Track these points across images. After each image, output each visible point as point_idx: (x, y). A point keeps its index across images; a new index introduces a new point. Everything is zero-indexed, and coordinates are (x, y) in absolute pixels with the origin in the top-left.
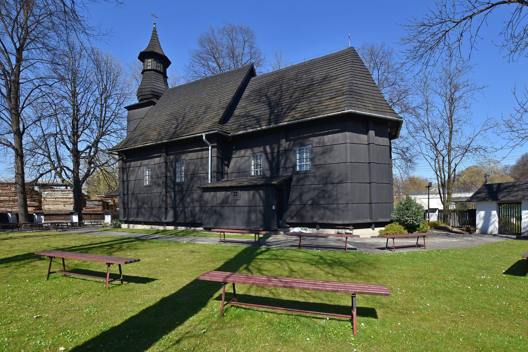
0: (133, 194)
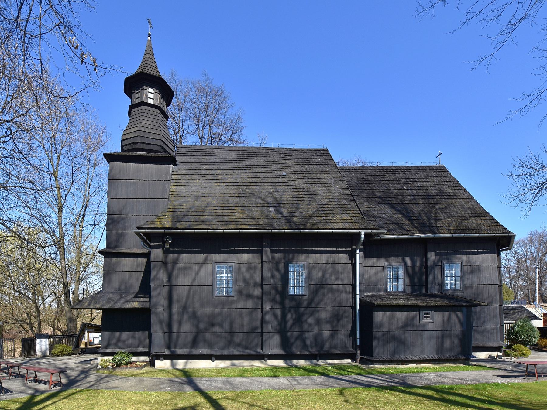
0: (185, 308)
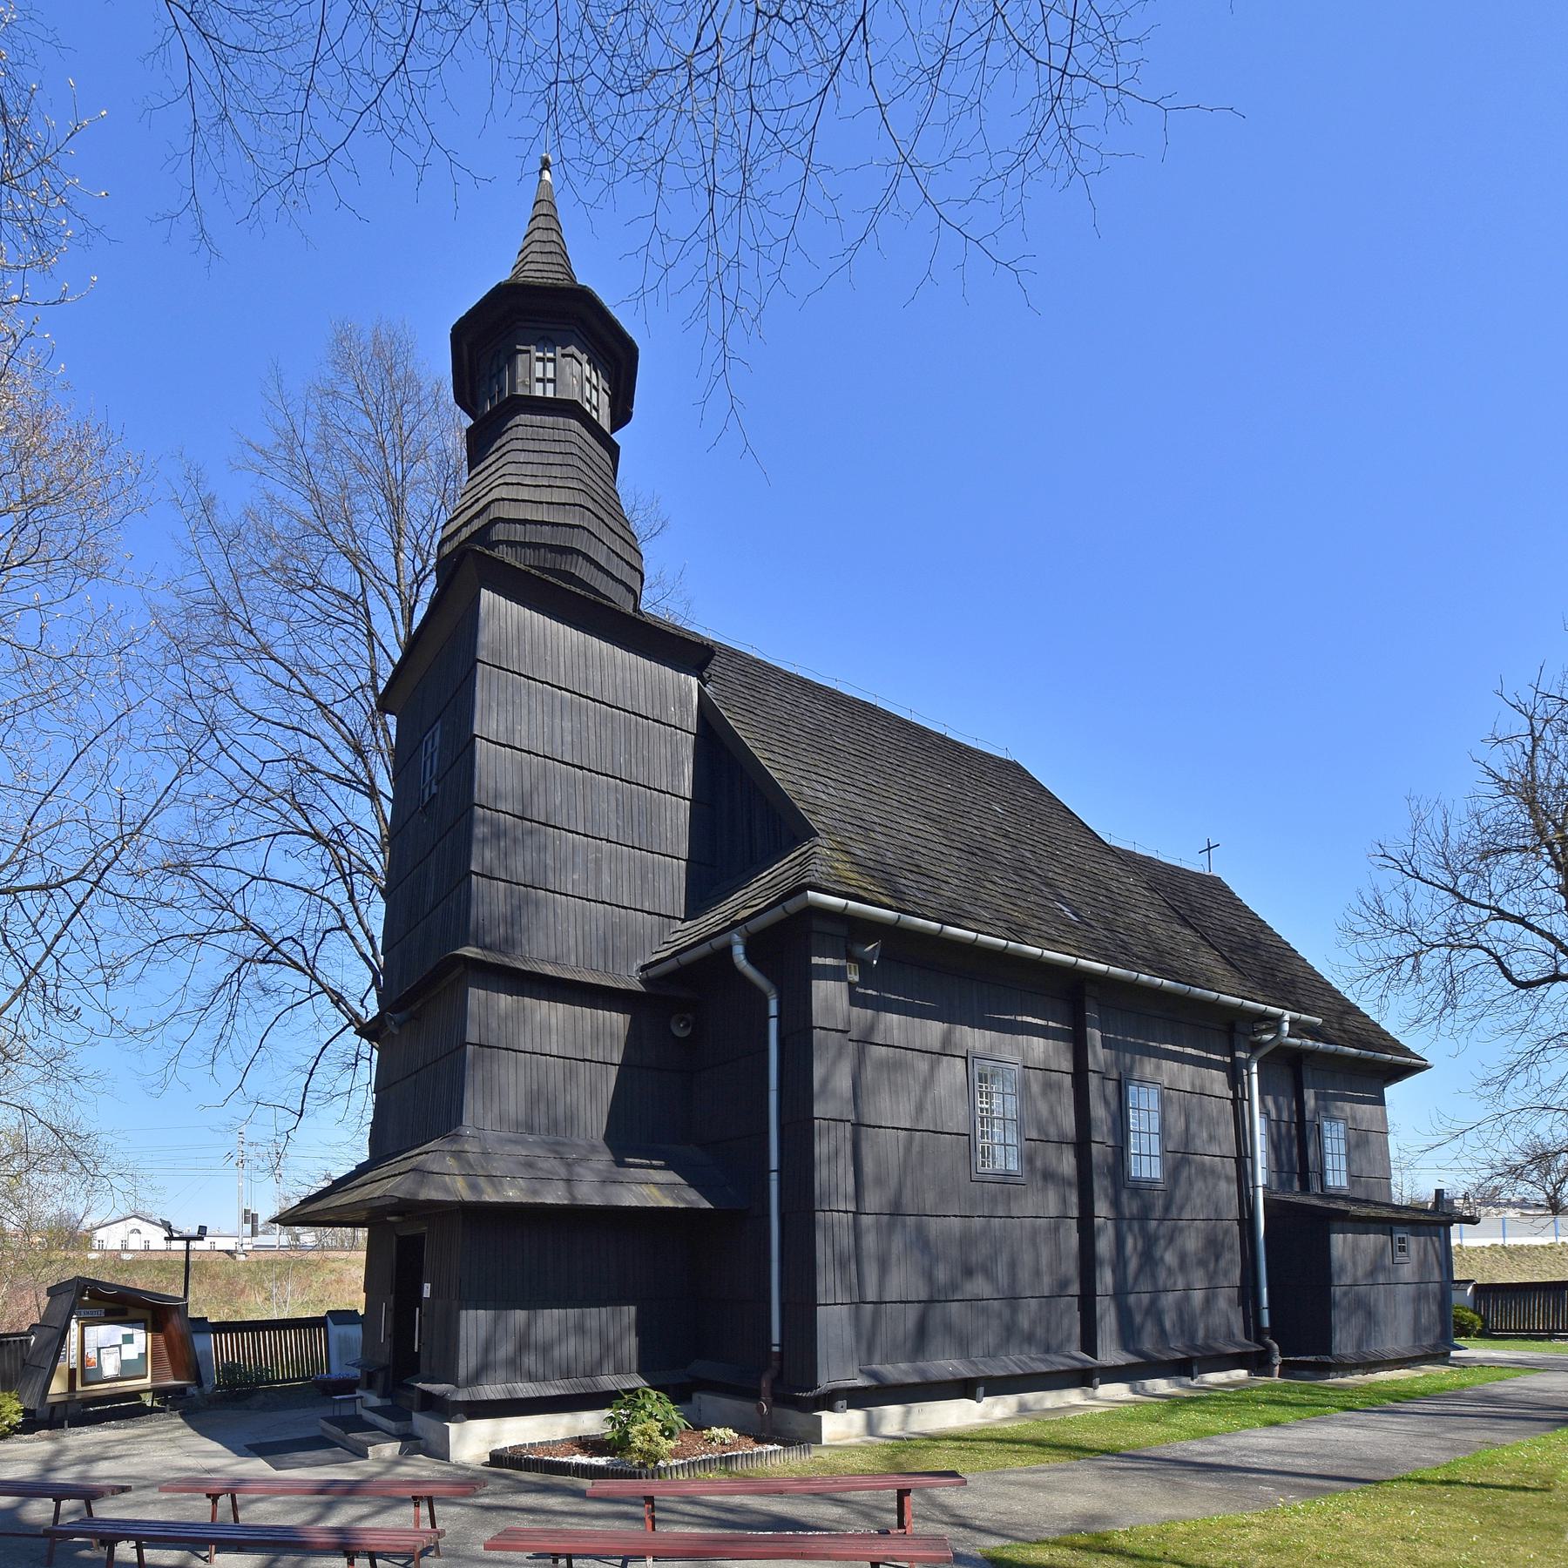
0: (896, 1212)
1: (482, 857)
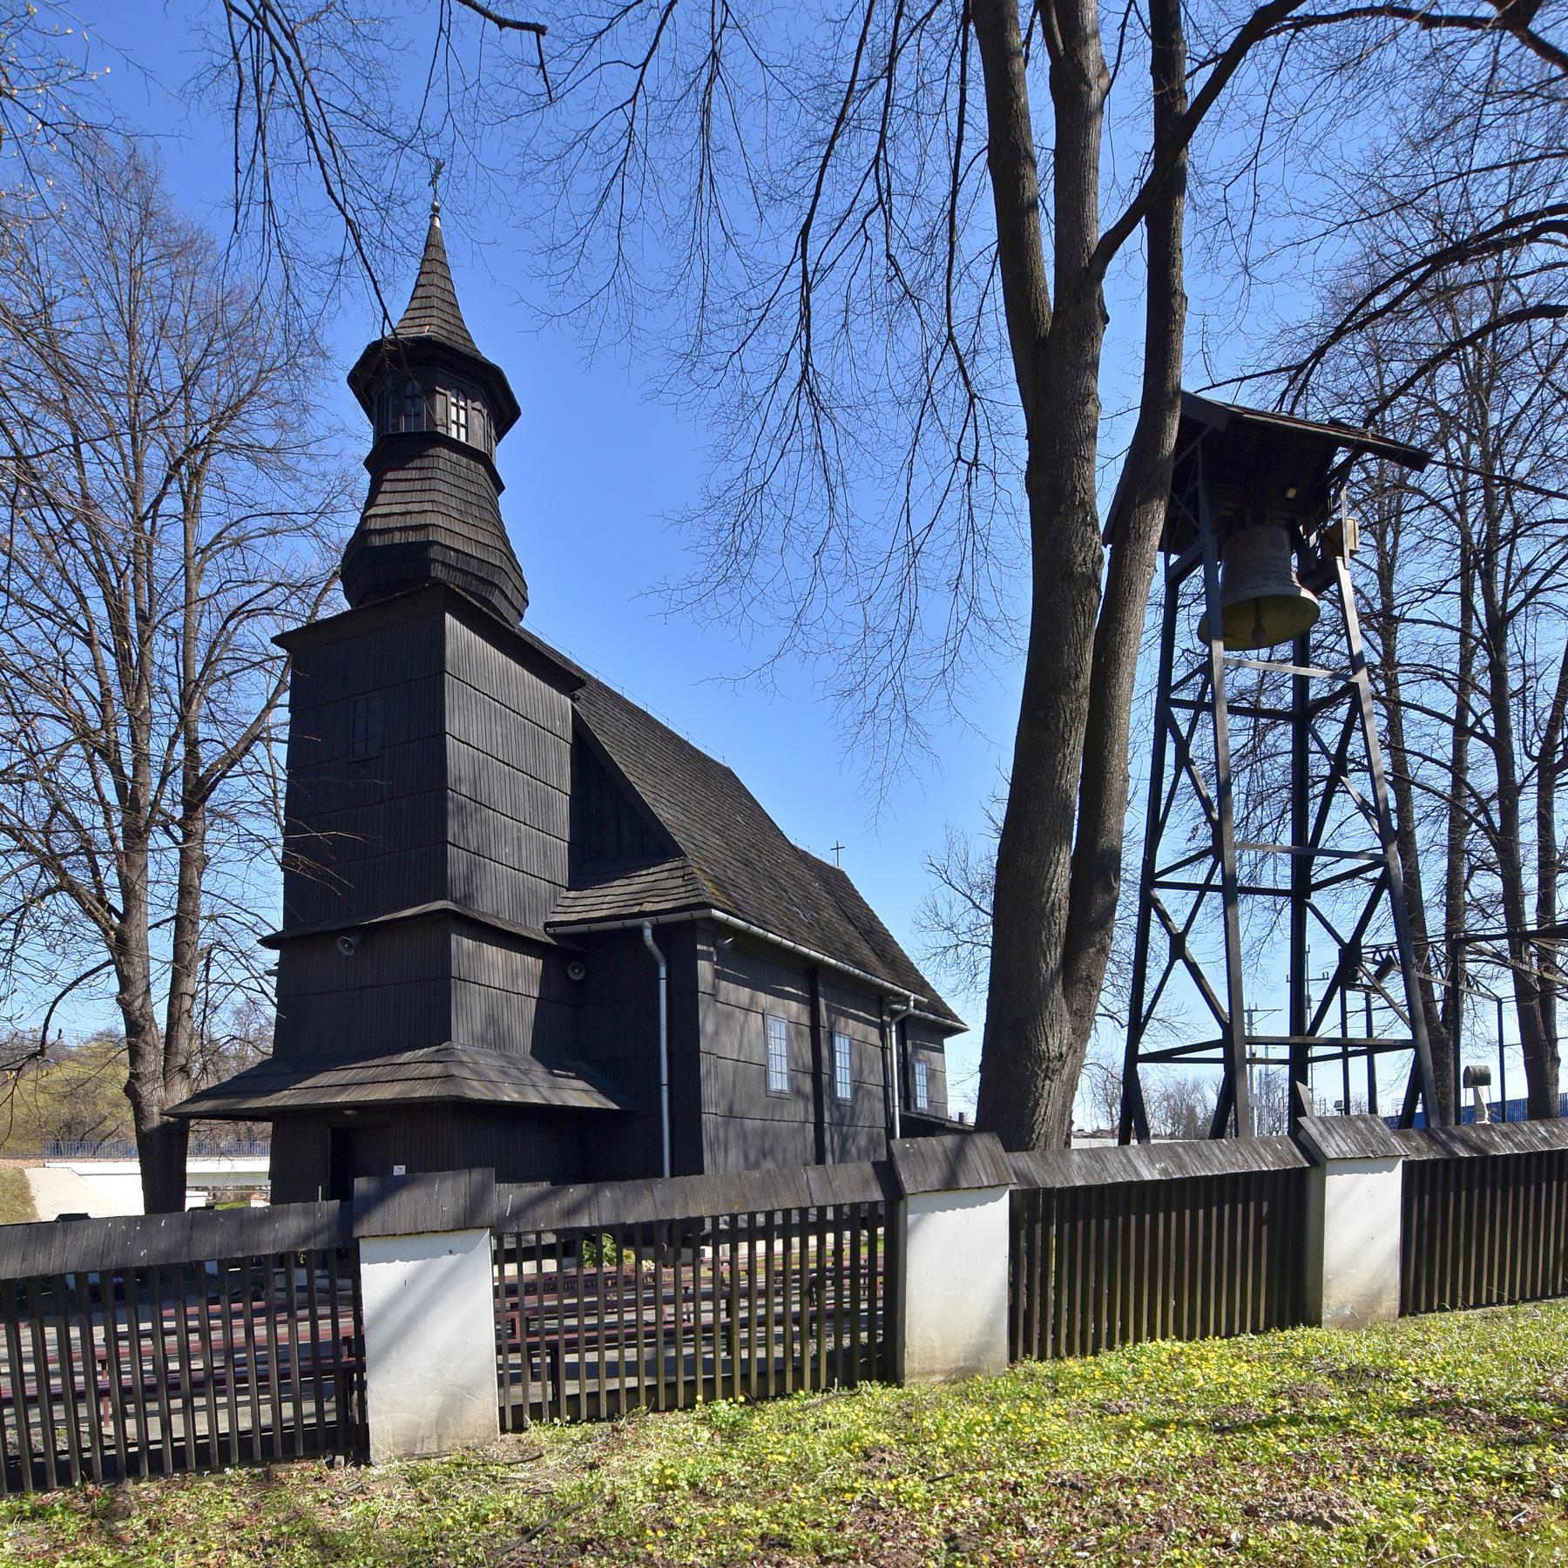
1: (453, 826)
